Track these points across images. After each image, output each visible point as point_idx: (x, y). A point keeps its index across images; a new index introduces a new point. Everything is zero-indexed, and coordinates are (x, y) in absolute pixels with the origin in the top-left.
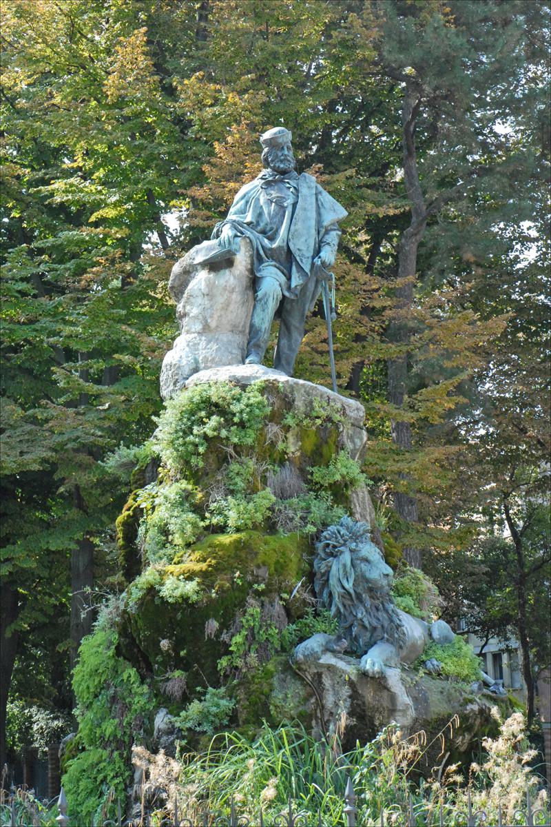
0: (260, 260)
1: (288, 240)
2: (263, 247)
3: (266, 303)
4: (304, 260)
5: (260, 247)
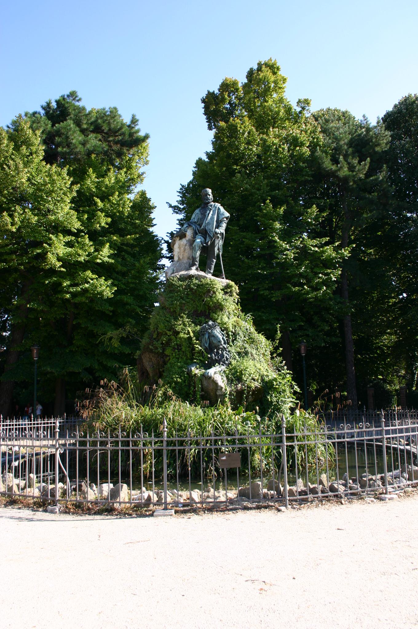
0: (197, 234)
1: (205, 226)
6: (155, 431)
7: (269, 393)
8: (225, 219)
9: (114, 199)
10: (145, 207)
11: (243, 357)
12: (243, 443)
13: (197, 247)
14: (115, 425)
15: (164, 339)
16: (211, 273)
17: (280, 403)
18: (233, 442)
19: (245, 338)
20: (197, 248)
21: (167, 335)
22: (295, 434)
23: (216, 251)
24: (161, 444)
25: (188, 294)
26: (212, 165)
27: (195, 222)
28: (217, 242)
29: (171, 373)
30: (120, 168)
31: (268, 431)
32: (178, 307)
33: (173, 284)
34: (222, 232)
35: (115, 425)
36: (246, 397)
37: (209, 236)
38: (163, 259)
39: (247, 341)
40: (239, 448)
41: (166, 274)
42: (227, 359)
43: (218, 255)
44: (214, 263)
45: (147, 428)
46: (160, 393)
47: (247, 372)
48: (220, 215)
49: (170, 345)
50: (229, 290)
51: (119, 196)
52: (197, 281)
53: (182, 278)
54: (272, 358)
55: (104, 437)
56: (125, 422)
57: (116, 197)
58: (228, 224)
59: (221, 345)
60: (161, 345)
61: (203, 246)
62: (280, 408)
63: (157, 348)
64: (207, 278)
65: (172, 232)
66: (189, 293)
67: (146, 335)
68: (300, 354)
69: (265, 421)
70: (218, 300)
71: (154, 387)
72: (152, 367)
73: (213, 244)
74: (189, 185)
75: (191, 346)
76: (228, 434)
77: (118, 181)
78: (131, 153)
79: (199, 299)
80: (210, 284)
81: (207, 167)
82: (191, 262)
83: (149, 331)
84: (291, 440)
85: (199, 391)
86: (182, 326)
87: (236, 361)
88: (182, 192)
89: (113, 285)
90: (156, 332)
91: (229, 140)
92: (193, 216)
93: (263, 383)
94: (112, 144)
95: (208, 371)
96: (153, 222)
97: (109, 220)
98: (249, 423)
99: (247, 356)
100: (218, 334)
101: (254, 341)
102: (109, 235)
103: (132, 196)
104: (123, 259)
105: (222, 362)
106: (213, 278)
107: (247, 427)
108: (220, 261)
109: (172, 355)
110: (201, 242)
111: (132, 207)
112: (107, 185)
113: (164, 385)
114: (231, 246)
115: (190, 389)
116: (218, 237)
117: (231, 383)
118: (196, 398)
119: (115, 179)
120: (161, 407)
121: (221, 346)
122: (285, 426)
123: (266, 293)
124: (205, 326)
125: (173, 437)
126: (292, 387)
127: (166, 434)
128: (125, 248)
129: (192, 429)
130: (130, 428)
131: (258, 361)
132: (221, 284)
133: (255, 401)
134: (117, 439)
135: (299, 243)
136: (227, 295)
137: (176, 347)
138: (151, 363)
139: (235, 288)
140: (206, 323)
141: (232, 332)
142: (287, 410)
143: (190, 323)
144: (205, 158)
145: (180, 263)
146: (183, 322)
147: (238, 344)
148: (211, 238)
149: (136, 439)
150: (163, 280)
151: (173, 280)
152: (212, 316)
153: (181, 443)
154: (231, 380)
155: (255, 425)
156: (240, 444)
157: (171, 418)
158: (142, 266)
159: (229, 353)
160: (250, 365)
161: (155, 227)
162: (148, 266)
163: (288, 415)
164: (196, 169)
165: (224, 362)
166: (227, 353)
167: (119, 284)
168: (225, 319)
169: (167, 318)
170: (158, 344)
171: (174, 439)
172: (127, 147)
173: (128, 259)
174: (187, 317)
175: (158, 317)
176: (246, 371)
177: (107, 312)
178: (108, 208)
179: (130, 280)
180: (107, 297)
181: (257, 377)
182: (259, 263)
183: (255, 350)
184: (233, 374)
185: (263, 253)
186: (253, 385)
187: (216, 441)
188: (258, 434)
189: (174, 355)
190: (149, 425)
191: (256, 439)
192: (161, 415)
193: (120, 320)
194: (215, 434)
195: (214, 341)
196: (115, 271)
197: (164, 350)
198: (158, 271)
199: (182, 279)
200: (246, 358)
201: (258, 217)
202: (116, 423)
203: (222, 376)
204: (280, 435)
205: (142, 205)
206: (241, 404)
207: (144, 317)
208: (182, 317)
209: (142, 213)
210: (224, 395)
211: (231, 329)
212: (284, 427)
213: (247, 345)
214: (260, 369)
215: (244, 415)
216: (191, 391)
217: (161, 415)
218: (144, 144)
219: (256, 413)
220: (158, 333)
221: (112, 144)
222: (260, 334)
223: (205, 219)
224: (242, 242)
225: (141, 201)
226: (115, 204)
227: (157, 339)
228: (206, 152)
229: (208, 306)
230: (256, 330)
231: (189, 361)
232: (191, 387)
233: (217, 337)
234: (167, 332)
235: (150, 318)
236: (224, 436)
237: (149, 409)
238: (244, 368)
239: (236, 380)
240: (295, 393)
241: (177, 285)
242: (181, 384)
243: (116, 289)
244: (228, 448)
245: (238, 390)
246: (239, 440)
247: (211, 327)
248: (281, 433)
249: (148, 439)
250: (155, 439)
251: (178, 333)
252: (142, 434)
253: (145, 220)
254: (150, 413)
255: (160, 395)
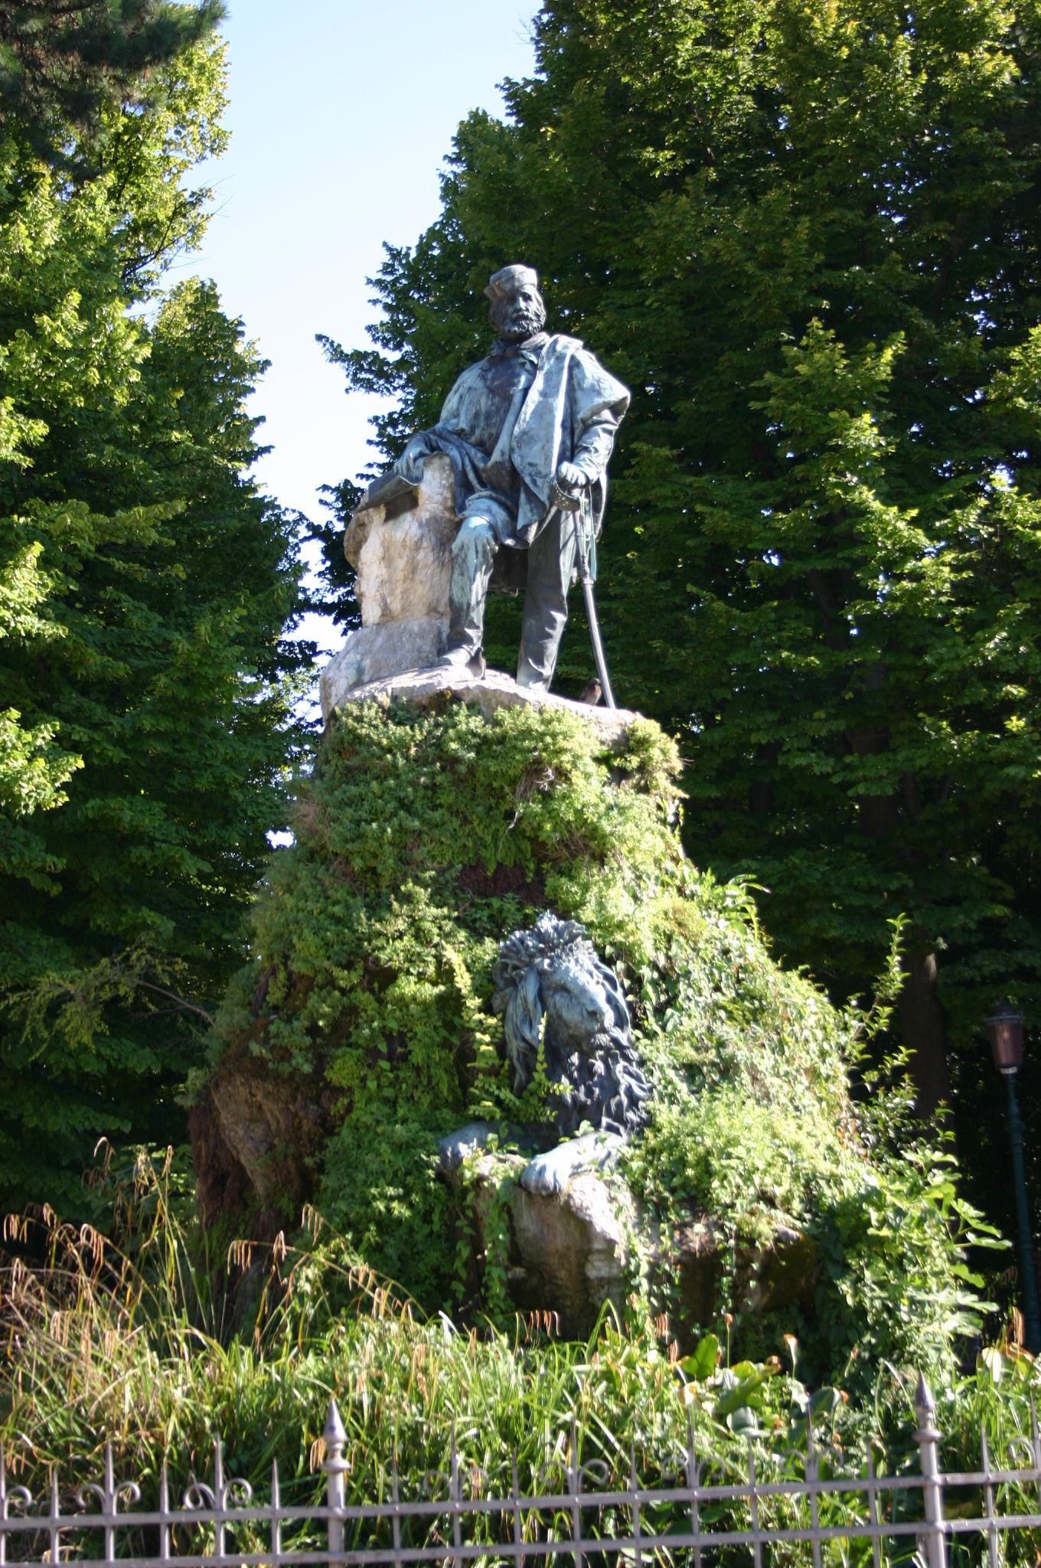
0: (469, 490)
1: (512, 450)
2: (475, 468)
3: (464, 561)
4: (539, 482)
5: (469, 468)
6: (287, 1473)
7: (848, 1266)
8: (607, 414)
9: (58, 329)
10: (215, 367)
11: (712, 1089)
12: (725, 1524)
13: (472, 554)
14: (84, 1446)
15: (323, 1008)
16: (545, 681)
17: (905, 1318)
18: (676, 1519)
19: (717, 996)
20: (473, 560)
21: (335, 987)
22: (989, 1474)
23: (567, 572)
24: (318, 1537)
25: (433, 787)
26: (536, 147)
27: (460, 433)
28: (568, 525)
29: (360, 1177)
30: (83, 174)
31: (848, 1458)
32: (388, 849)
33: (359, 739)
34: (593, 477)
35: (84, 1446)
36: (734, 1287)
37: (532, 497)
38: (309, 616)
39: (731, 1007)
40: (706, 1549)
41: (326, 687)
42: (634, 1101)
43: (577, 589)
44: (558, 632)
45: (245, 1459)
46: (307, 1277)
47: (733, 1162)
48: (579, 394)
49: (349, 1035)
50: (634, 761)
51: (84, 312)
52: (476, 723)
53: (403, 708)
54: (858, 1093)
55: (31, 1511)
56: (133, 1426)
57: (69, 315)
58: (622, 438)
59: (604, 1030)
60: (308, 1040)
61: (503, 547)
62: (903, 1341)
63: (285, 1055)
64: (523, 702)
65: (347, 482)
66: (439, 779)
67: (234, 989)
68: (992, 1067)
69: (830, 1408)
70: (579, 813)
71: (280, 1245)
72: (262, 1149)
73: (550, 536)
74: (423, 247)
75: (455, 1040)
76: (651, 1478)
77: (74, 237)
78: (138, 95)
79: (490, 809)
80: (543, 735)
81: (512, 158)
82: (446, 630)
83: (246, 969)
84: (969, 1506)
85: (498, 1265)
86: (407, 941)
87: (676, 1109)
88: (394, 282)
89: (63, 744)
90: (282, 975)
91: (619, 21)
92: (452, 402)
93: (815, 1215)
94: (39, 49)
95: (541, 1160)
96: (254, 439)
97: (40, 429)
98: (752, 1418)
99: (731, 1081)
100: (583, 978)
101: (762, 1009)
102: (36, 502)
103: (147, 312)
104: (113, 617)
105: (609, 1114)
106: (556, 703)
107: (743, 1439)
108: (587, 620)
109: (364, 1087)
110: (492, 527)
111: (146, 367)
112: (22, 256)
113: (325, 1238)
114: (637, 543)
115: (452, 1253)
116: (575, 505)
117: (657, 1219)
118: (485, 1300)
119: (61, 226)
120: (312, 1345)
121: (603, 1039)
122: (937, 1434)
123: (821, 764)
124: (522, 941)
125: (374, 1499)
126: (956, 1227)
127: (340, 1484)
128: (119, 565)
129: (469, 1455)
130: (159, 1456)
131: (785, 1111)
132: (594, 730)
133: (776, 1305)
134: (95, 1520)
135: (973, 518)
136: (627, 785)
137: (383, 1047)
138: (259, 1131)
139: (664, 752)
140: (527, 923)
141: (654, 966)
142: (938, 1350)
143: (448, 926)
144: (500, 113)
145: (390, 636)
146: (414, 922)
147: (687, 1025)
148: (541, 508)
149: (192, 1518)
150: (311, 719)
151: (359, 719)
152: (555, 889)
153: (418, 1530)
154: (656, 1204)
155: (784, 1432)
156: (710, 1527)
157: (366, 1401)
158: (206, 652)
159: (641, 1072)
160: (748, 1128)
161: (263, 459)
162: (237, 650)
163: (946, 1378)
164: (459, 169)
165: (619, 1117)
166: (634, 1068)
167: (92, 740)
168: (619, 904)
169: (334, 904)
170: (291, 1034)
171: (380, 1511)
172: (114, 64)
173: (136, 620)
174: (431, 897)
175: (289, 901)
176: (729, 1156)
177: (36, 882)
178: (31, 372)
179: (147, 724)
180: (38, 807)
181: (786, 1186)
182: (780, 624)
183: (767, 1052)
184: (664, 1176)
185: (797, 567)
186: (763, 1227)
187: (591, 1517)
188: (801, 1473)
189: (372, 1085)
190: (255, 1441)
191: (792, 1502)
192: (314, 1387)
193: (100, 920)
194: (586, 1479)
195: (565, 1014)
196: (72, 682)
197: (321, 1062)
198: (281, 674)
199: (402, 711)
200: (726, 1094)
201: (772, 401)
202: (87, 1433)
203: (610, 1184)
204: (911, 1481)
205: (198, 352)
206: (709, 1323)
207: (220, 901)
208: (408, 899)
209: (199, 392)
210: (624, 1282)
211: (648, 951)
212: (932, 1439)
213: (727, 1031)
214: (796, 1148)
215: (729, 1377)
216: (458, 1264)
217: (314, 1387)
218: (202, 52)
219: (786, 1368)
220: (292, 982)
221: (41, 54)
222: (793, 975)
223: (510, 418)
224: (693, 525)
225: (197, 338)
226: (65, 353)
227: (287, 1010)
228: (508, 80)
229: (534, 840)
230: (774, 956)
231: (446, 1114)
232: (460, 1245)
233: (583, 991)
234: (338, 972)
235: (247, 907)
236: (634, 1494)
237: (256, 1360)
238: (721, 1142)
239: (680, 1203)
240: (978, 1259)
241: (379, 744)
242: (411, 1230)
243: (81, 764)
244: (650, 1552)
245: (689, 1253)
246: (707, 1506)
247: (550, 945)
248: (916, 1470)
249: (253, 1515)
250: (286, 1511)
251: (390, 976)
252: (221, 1490)
253: (215, 430)
254: (260, 1378)
255: (307, 1287)
